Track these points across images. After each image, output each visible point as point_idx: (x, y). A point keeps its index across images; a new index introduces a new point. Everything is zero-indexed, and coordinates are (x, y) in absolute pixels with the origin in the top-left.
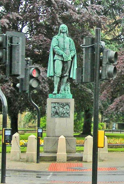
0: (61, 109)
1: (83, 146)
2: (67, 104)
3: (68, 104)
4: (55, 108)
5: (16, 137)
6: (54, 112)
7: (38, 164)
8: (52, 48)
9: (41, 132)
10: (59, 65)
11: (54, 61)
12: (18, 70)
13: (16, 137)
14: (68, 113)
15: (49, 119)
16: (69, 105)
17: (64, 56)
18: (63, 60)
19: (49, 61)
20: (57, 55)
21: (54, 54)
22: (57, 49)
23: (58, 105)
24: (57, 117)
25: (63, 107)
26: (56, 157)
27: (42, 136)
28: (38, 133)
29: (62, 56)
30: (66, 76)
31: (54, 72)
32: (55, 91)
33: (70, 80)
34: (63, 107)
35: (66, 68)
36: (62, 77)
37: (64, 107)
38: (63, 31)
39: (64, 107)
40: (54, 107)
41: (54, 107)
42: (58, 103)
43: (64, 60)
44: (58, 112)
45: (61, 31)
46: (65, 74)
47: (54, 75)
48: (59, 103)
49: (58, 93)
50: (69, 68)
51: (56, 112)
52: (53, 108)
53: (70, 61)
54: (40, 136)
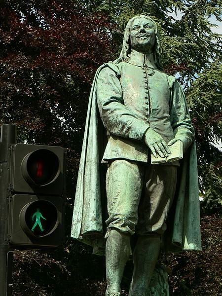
22: (117, 112)
53: (174, 170)
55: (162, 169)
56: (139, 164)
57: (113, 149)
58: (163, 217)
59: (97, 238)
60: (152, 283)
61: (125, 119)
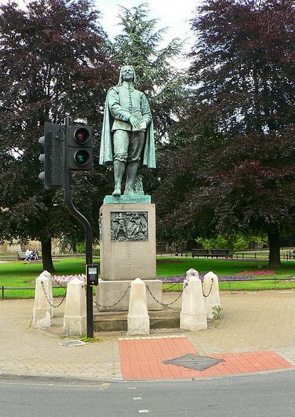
0: (130, 225)
1: (158, 261)
2: (143, 215)
3: (143, 215)
4: (119, 223)
5: (42, 283)
7: (91, 347)
9: (96, 273)
10: (121, 140)
11: (112, 133)
12: (17, 376)
13: (42, 283)
14: (144, 233)
15: (110, 251)
16: (145, 216)
18: (129, 129)
20: (118, 122)
21: (112, 120)
22: (118, 109)
25: (134, 221)
27: (96, 283)
29: (128, 122)
31: (113, 154)
32: (117, 191)
33: (142, 169)
34: (134, 221)
37: (136, 221)
38: (128, 77)
39: (136, 221)
40: (117, 221)
41: (117, 221)
42: (124, 213)
43: (133, 129)
44: (125, 231)
45: (124, 77)
46: (134, 157)
47: (113, 159)
49: (122, 193)
52: (114, 224)
54: (91, 282)
55: (137, 133)
56: (128, 131)
57: (116, 125)
58: (139, 154)
59: (110, 163)
60: (135, 182)
61: (121, 112)
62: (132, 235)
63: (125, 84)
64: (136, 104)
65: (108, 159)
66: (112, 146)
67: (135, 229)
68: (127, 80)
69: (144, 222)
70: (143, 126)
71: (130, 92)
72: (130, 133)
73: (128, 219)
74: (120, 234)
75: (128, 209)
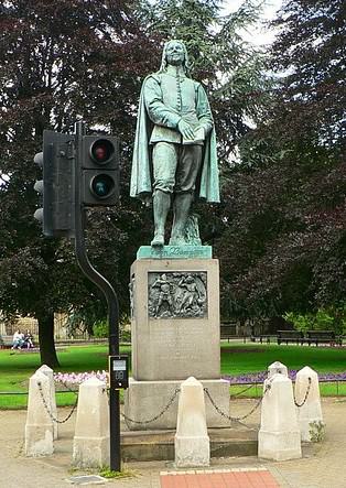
2: (199, 277)
6: (156, 302)
8: (143, 109)
10: (165, 157)
11: (151, 147)
14: (200, 305)
15: (148, 334)
17: (181, 129)
18: (177, 141)
19: (135, 149)
20: (160, 129)
21: (150, 126)
22: (159, 109)
23: (171, 280)
24: (166, 318)
26: (322, 396)
27: (126, 385)
28: (113, 373)
29: (175, 129)
30: (189, 192)
31: (152, 180)
32: (159, 238)
33: (198, 204)
35: (188, 168)
36: (175, 194)
37: (189, 286)
38: (176, 58)
39: (189, 286)
40: (158, 287)
41: (158, 287)
42: (169, 274)
43: (184, 141)
44: (170, 302)
46: (185, 185)
47: (153, 188)
48: (171, 272)
49: (167, 243)
50: (197, 167)
51: (165, 302)
52: (153, 291)
54: (118, 384)
55: (191, 147)
56: (175, 144)
57: (156, 135)
58: (193, 180)
59: (147, 195)
60: (187, 224)
61: (164, 114)
62: (182, 307)
63: (172, 69)
64: (188, 102)
65: (144, 188)
66: (150, 167)
67: (187, 300)
68: (175, 64)
69: (201, 288)
70: (200, 136)
71: (179, 82)
72: (179, 147)
73: (176, 283)
74: (163, 307)
75: (175, 267)
